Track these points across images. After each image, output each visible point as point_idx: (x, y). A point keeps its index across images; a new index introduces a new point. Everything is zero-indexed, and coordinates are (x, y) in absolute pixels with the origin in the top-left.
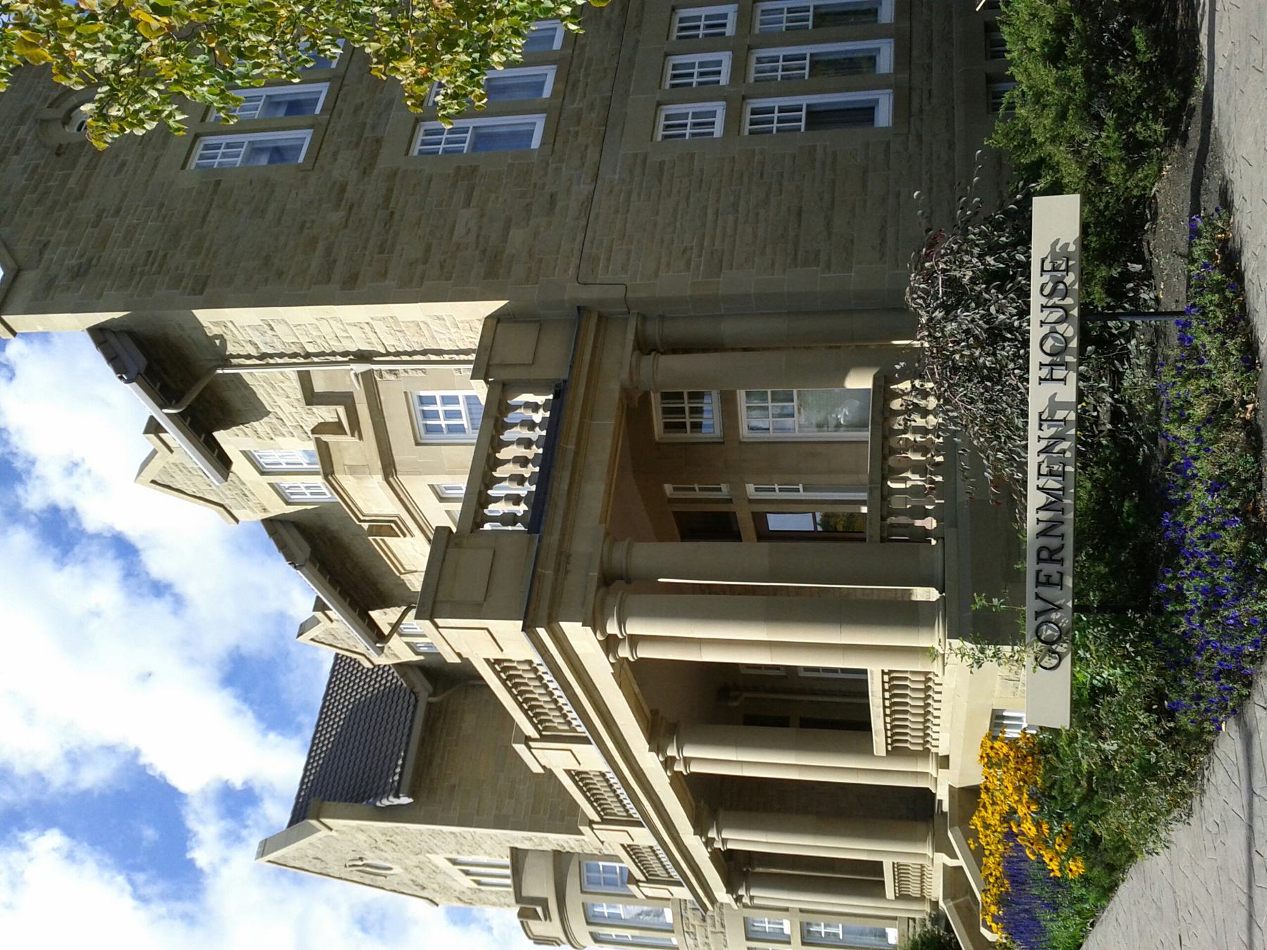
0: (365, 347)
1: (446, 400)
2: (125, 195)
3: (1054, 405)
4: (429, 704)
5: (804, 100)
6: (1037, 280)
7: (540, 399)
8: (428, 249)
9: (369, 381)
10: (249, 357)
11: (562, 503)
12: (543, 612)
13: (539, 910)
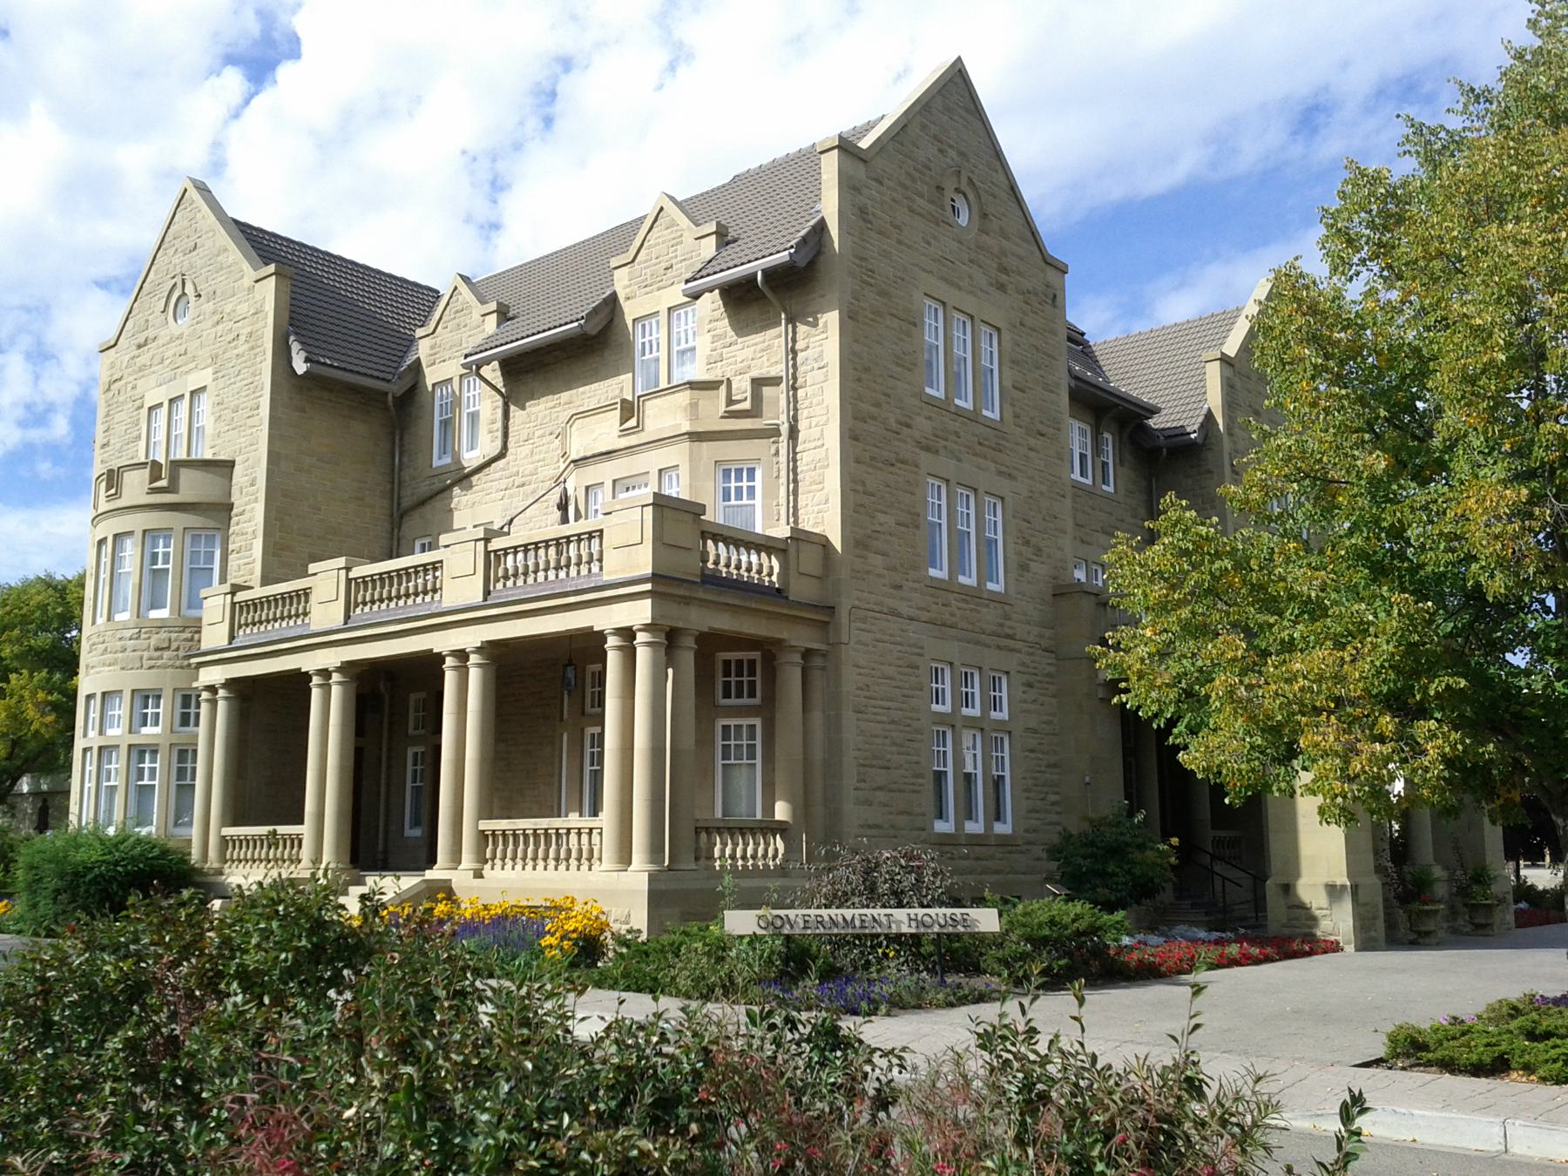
1: (751, 490)
2: (909, 247)
3: (899, 923)
5: (950, 769)
6: (958, 911)
7: (774, 578)
9: (774, 432)
10: (794, 340)
11: (722, 599)
12: (662, 589)
13: (163, 483)
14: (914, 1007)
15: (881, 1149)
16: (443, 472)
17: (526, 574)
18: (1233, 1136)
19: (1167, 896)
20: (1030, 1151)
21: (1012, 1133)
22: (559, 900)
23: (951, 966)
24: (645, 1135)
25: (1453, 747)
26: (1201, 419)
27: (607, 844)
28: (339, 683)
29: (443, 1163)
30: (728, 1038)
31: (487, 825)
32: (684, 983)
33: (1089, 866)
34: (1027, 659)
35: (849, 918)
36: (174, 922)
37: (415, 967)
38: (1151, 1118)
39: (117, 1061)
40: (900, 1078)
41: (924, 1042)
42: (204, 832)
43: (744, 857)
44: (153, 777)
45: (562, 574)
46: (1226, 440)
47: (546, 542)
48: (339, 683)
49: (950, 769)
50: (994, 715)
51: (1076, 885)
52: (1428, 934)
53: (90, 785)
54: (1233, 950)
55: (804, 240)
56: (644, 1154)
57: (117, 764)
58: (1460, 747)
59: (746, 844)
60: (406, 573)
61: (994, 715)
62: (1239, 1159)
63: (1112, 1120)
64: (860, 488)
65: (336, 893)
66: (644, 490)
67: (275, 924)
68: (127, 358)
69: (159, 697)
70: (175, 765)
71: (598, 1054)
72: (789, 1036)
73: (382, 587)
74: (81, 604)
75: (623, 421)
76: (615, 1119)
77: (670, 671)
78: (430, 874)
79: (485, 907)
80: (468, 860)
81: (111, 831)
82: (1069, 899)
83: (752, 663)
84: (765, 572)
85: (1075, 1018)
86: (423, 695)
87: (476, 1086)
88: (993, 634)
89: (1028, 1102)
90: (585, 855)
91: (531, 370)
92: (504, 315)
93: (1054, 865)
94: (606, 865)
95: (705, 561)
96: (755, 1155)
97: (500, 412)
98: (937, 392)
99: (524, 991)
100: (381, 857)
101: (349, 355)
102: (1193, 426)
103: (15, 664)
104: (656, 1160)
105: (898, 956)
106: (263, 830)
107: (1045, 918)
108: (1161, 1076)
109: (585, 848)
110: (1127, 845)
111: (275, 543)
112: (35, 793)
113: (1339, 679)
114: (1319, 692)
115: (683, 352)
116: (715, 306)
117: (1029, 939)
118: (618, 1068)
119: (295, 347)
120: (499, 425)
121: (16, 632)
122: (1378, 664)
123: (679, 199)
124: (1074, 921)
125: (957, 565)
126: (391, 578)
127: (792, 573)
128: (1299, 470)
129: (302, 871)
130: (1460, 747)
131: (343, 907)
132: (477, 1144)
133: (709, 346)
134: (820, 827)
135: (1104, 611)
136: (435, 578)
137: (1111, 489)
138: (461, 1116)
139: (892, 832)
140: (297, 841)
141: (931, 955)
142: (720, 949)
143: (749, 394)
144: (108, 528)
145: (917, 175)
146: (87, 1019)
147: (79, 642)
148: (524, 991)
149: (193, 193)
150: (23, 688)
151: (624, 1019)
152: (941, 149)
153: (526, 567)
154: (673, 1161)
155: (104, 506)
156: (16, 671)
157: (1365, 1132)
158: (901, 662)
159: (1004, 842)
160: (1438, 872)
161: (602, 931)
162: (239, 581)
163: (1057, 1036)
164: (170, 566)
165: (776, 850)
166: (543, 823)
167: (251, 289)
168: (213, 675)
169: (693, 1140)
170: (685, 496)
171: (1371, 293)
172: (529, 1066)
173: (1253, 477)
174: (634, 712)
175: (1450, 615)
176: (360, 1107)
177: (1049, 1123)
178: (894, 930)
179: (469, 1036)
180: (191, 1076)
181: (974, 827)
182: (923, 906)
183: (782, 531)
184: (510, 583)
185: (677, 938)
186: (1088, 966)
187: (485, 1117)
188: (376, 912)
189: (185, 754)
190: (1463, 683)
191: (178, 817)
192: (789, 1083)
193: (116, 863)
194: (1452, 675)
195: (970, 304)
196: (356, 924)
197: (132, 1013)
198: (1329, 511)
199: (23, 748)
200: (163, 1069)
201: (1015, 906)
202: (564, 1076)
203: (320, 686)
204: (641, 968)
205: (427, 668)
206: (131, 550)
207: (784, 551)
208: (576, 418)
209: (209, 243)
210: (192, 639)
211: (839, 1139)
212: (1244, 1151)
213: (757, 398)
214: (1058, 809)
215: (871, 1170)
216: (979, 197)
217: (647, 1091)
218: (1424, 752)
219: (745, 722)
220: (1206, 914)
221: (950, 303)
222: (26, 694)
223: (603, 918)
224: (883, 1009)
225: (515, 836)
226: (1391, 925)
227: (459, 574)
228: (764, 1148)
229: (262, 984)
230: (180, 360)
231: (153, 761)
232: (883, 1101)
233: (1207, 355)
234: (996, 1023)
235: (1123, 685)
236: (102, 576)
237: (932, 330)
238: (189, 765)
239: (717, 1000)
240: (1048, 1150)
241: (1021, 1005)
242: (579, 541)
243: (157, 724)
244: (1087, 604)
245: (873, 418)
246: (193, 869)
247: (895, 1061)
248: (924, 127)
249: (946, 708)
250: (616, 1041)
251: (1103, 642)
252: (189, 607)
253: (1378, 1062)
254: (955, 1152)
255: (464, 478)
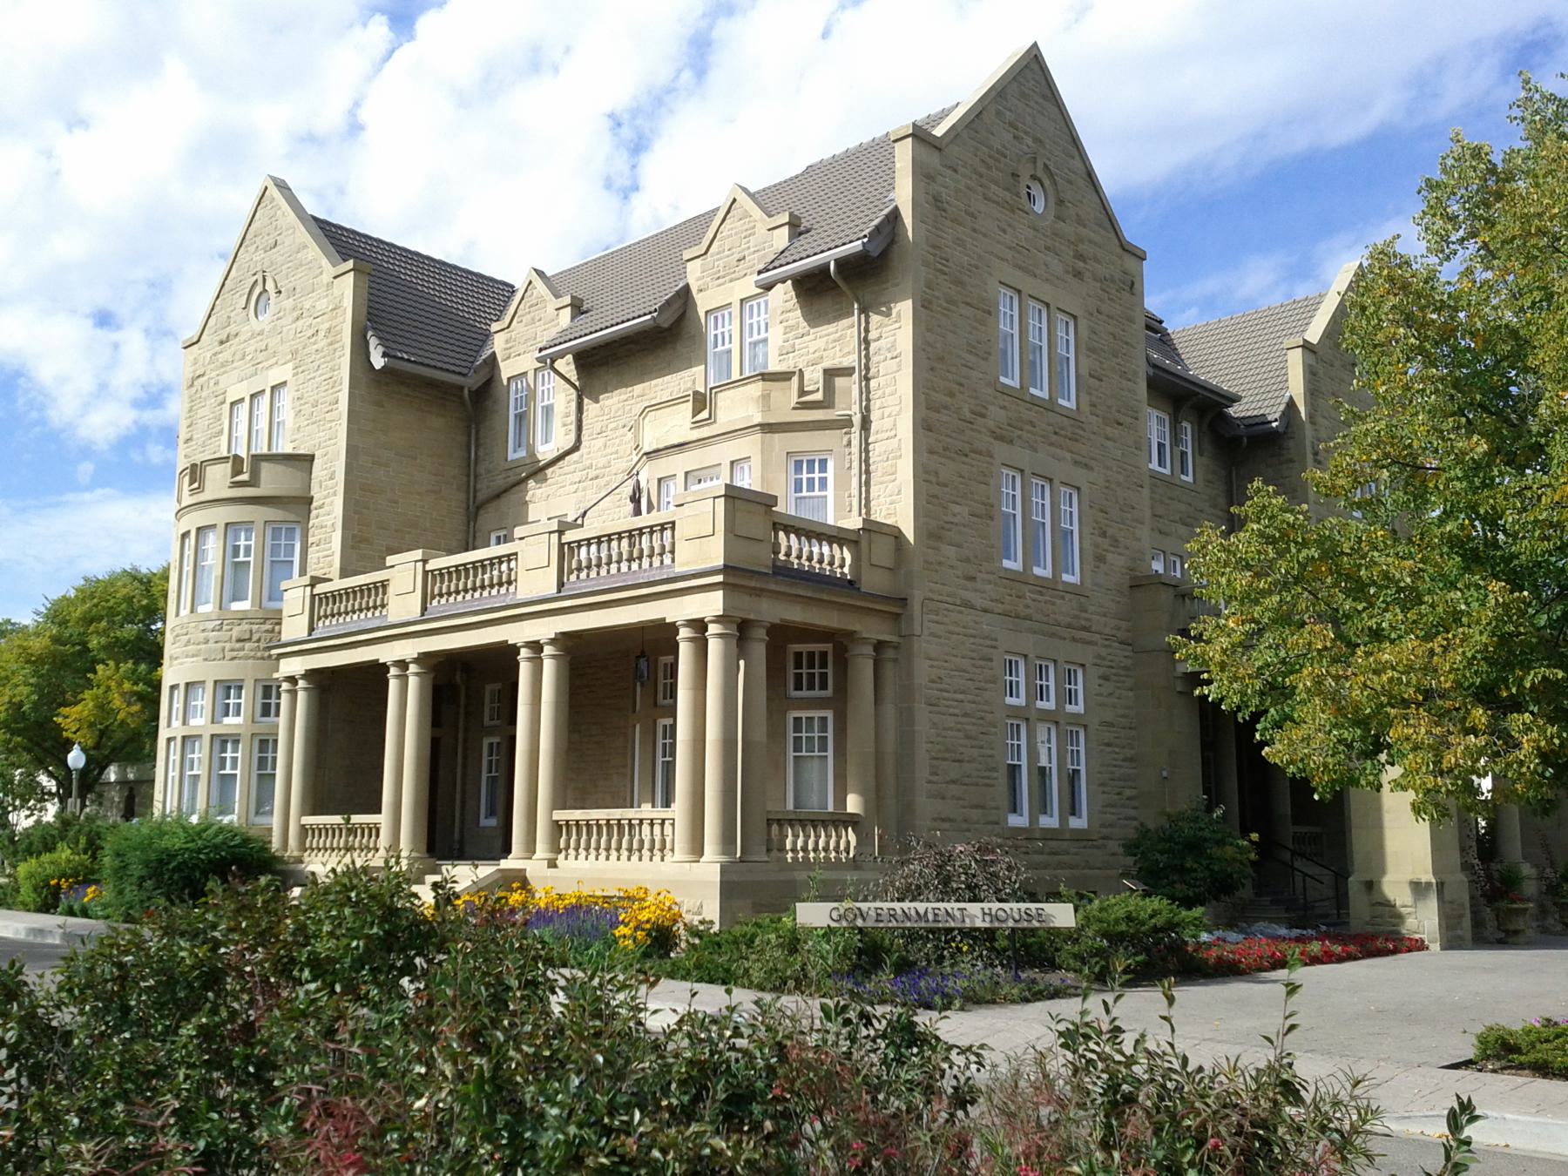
0: (873, 426)
1: (823, 482)
3: (973, 917)
4: (461, 388)
5: (1024, 763)
6: (1033, 906)
7: (846, 570)
8: (946, 485)
9: (846, 423)
10: (867, 331)
11: (793, 591)
12: (731, 580)
13: (245, 477)
14: (988, 1002)
15: (961, 1148)
16: (519, 465)
17: (599, 566)
18: (1332, 1142)
19: (1246, 893)
20: (1116, 1155)
21: (1098, 1134)
22: (633, 892)
23: (1026, 962)
24: (717, 1132)
25: (1550, 741)
26: (1282, 407)
27: (680, 835)
28: (417, 674)
29: (513, 1156)
30: (802, 1033)
31: (561, 815)
32: (757, 976)
33: (1167, 861)
34: (1103, 652)
35: (922, 912)
36: (251, 908)
37: (488, 951)
38: (1247, 1124)
39: (191, 1048)
40: (981, 1078)
41: (1002, 1037)
42: (285, 821)
43: (816, 850)
44: (234, 767)
45: (635, 566)
46: (1308, 428)
47: (619, 534)
48: (417, 674)
49: (1024, 763)
50: (1070, 708)
51: (1153, 879)
52: (1516, 932)
53: (174, 774)
54: (1315, 947)
55: (878, 228)
56: (716, 1152)
57: (200, 754)
58: (1556, 741)
59: (818, 837)
60: (481, 565)
61: (1070, 708)
62: (1339, 1167)
63: (1203, 1125)
64: (933, 479)
65: (409, 882)
66: (715, 482)
67: (347, 911)
68: (209, 355)
69: (241, 688)
70: (256, 755)
71: (671, 1047)
72: (864, 1032)
73: (458, 579)
74: (166, 597)
75: (696, 413)
76: (687, 1114)
77: (742, 663)
78: (505, 864)
79: (560, 897)
80: (542, 850)
81: (194, 819)
82: (1147, 894)
83: (824, 655)
84: (837, 563)
85: (1164, 1018)
86: (498, 686)
87: (548, 1078)
88: (1069, 626)
89: (1114, 1104)
90: (657, 846)
91: (605, 362)
92: (578, 308)
93: (1130, 860)
94: (678, 855)
95: (776, 553)
96: (830, 1153)
97: (574, 405)
98: (1012, 381)
99: (596, 982)
100: (457, 846)
101: (426, 353)
102: (1274, 414)
103: (102, 655)
104: (729, 1159)
105: (972, 949)
106: (337, 819)
107: (1121, 913)
108: (1255, 1079)
109: (658, 838)
110: (1205, 840)
111: (354, 536)
112: (122, 782)
113: (1429, 669)
114: (1408, 684)
115: (755, 344)
116: (788, 296)
117: (1105, 935)
118: (691, 1063)
119: (373, 342)
120: (573, 418)
121: (104, 624)
122: (1469, 655)
123: (752, 191)
124: (1151, 917)
125: (1031, 556)
126: (467, 570)
128: (1387, 455)
129: (377, 861)
130: (1556, 741)
131: (416, 896)
132: (547, 1139)
133: (781, 338)
134: (892, 823)
135: (1185, 602)
136: (510, 570)
137: (1190, 479)
138: (532, 1109)
139: (965, 826)
140: (375, 830)
141: (1005, 950)
142: (793, 942)
143: (821, 385)
144: (192, 522)
145: (991, 162)
146: (163, 1005)
147: (163, 634)
148: (596, 982)
149: (274, 192)
150: (109, 678)
151: (696, 1012)
152: (1017, 135)
153: (600, 558)
154: (747, 1161)
155: (187, 500)
156: (103, 662)
157: (1474, 1139)
158: (974, 655)
159: (1078, 837)
160: (1527, 870)
161: (675, 921)
162: (319, 574)
163: (1143, 1035)
164: (251, 559)
165: (848, 843)
166: (616, 813)
167: (330, 286)
168: (294, 666)
169: (768, 1137)
170: (757, 487)
171: (1469, 272)
172: (600, 1059)
173: (1342, 457)
174: (706, 702)
175: (1545, 605)
176: (430, 1098)
177: (1137, 1125)
178: (968, 924)
179: (540, 1027)
180: (266, 1064)
181: (1049, 822)
182: (1000, 901)
183: (854, 522)
184: (583, 575)
185: (749, 929)
186: (1167, 962)
187: (555, 1111)
188: (448, 901)
189: (266, 744)
190: (1560, 675)
191: (260, 804)
192: (866, 1081)
193: (199, 851)
194: (1548, 667)
195: (1047, 292)
196: (428, 913)
197: (207, 1000)
198: (1421, 499)
199: (110, 738)
200: (242, 1058)
201: (1091, 901)
202: (634, 1072)
203: (397, 677)
204: (714, 960)
205: (501, 661)
206: (213, 543)
207: (856, 542)
208: (650, 410)
209: (288, 241)
210: (273, 631)
211: (918, 1139)
212: (1344, 1159)
213: (829, 388)
214: (1135, 803)
215: (951, 1171)
217: (723, 1087)
218: (1518, 746)
219: (816, 714)
220: (1287, 911)
221: (1026, 290)
222: (113, 684)
223: (676, 909)
224: (957, 1003)
225: (588, 826)
226: (1478, 924)
227: (532, 564)
228: (840, 1147)
229: (334, 972)
230: (261, 357)
231: (235, 750)
232: (963, 1098)
233: (1288, 342)
234: (1078, 1021)
235: (1206, 676)
236: (185, 569)
237: (1007, 318)
238: (270, 755)
239: (790, 993)
240: (1135, 1152)
241: (1105, 1003)
242: (652, 533)
243: (238, 714)
244: (1166, 596)
245: (945, 407)
246: (275, 858)
247: (973, 1058)
248: (998, 114)
249: (1021, 701)
250: (689, 1035)
251: (1184, 632)
252: (270, 599)
253: (1467, 1064)
254: (1039, 1156)
255: (538, 471)
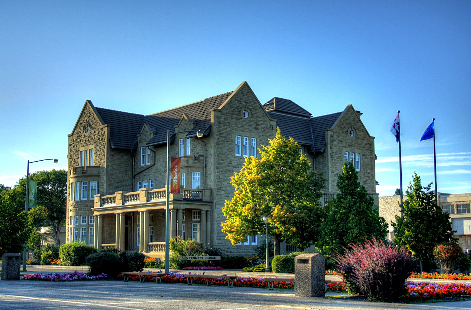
16: (143, 167)
127: (203, 196)
149: (89, 104)
216: (251, 110)
221: (242, 135)
